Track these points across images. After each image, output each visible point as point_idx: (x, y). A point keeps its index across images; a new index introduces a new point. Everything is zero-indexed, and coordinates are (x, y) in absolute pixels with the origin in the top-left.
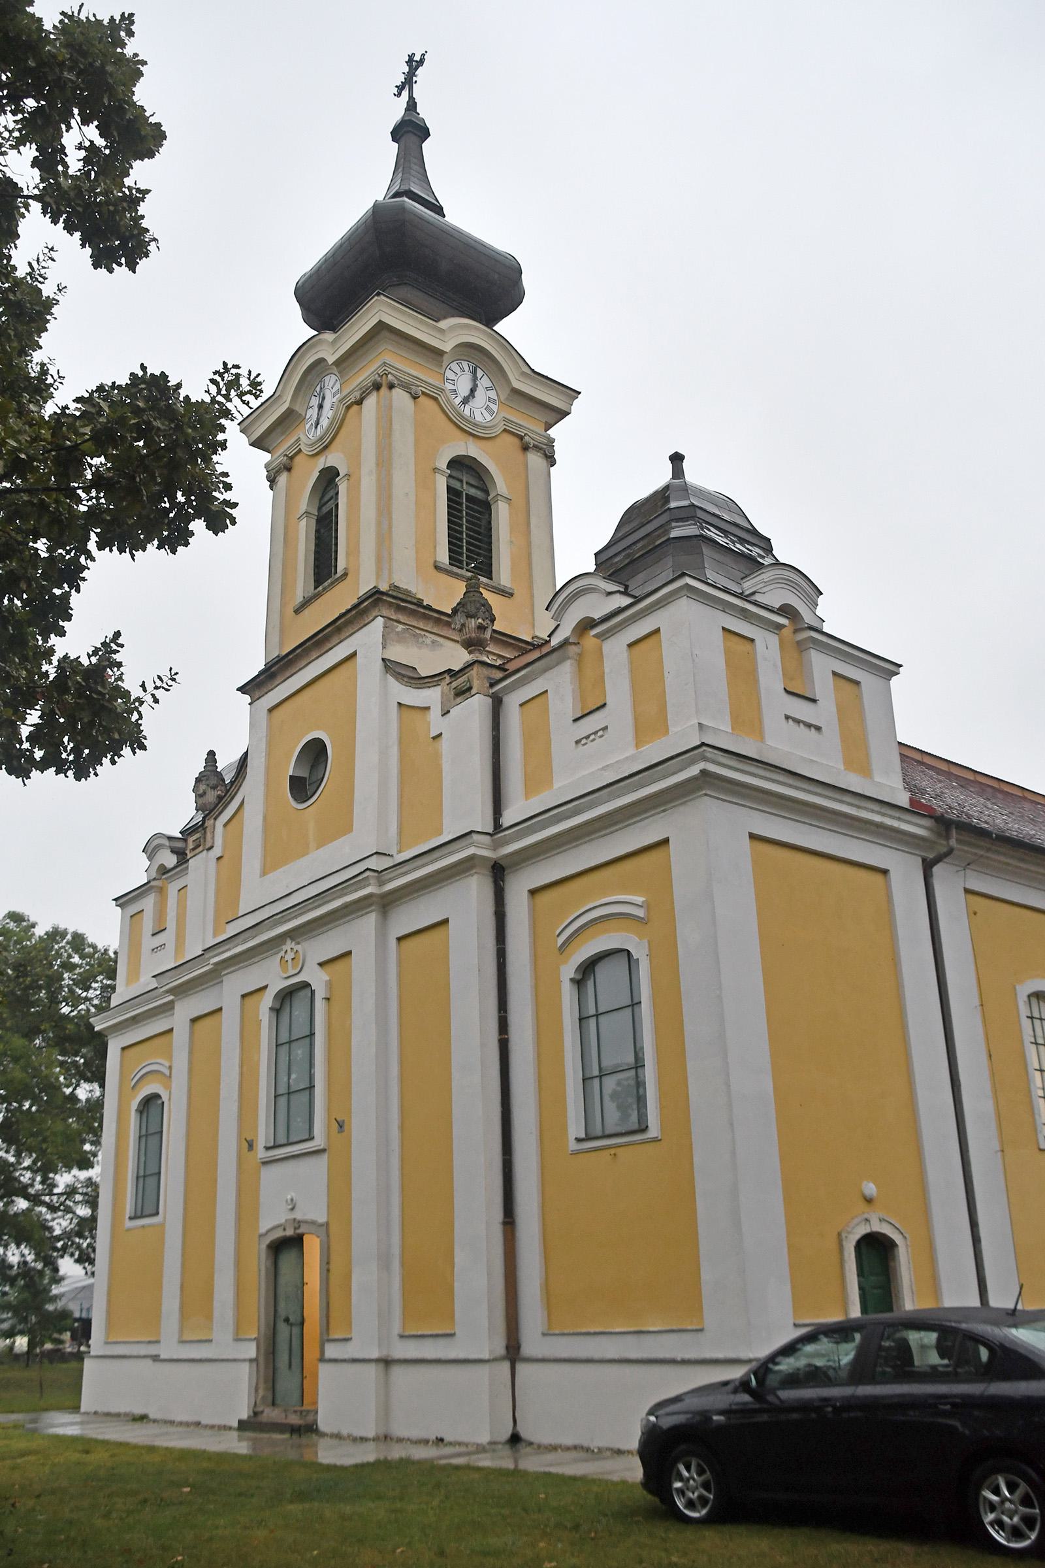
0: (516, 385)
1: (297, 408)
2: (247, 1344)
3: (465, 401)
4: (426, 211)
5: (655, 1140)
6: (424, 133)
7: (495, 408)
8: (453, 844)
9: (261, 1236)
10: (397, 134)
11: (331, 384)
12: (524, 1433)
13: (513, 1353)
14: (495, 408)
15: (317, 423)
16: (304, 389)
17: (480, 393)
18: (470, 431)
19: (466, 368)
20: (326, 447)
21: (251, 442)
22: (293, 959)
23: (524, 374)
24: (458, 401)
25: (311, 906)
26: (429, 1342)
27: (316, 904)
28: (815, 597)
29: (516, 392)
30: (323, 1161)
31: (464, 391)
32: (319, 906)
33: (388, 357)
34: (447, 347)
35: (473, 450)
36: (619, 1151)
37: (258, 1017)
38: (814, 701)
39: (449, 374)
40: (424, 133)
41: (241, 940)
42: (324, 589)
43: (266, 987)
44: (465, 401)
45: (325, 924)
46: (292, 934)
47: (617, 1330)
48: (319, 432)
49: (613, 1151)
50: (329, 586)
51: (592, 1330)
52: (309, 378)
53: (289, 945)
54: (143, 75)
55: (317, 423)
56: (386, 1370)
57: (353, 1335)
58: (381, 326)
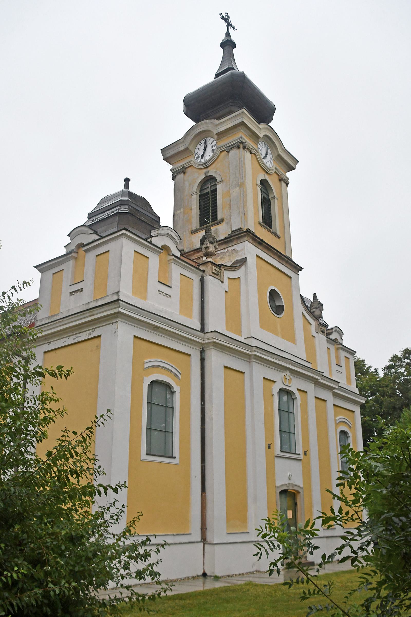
0: (280, 153)
1: (190, 148)
3: (264, 158)
4: (224, 75)
6: (234, 45)
10: (223, 45)
11: (210, 142)
12: (201, 573)
13: (204, 540)
15: (202, 156)
17: (268, 155)
18: (266, 171)
19: (264, 145)
21: (164, 158)
23: (283, 149)
24: (262, 157)
25: (304, 368)
27: (305, 369)
29: (279, 156)
31: (264, 154)
32: (305, 370)
33: (242, 135)
34: (261, 135)
35: (267, 177)
39: (259, 146)
40: (234, 45)
44: (264, 158)
45: (301, 376)
48: (203, 160)
55: (202, 156)
58: (243, 124)
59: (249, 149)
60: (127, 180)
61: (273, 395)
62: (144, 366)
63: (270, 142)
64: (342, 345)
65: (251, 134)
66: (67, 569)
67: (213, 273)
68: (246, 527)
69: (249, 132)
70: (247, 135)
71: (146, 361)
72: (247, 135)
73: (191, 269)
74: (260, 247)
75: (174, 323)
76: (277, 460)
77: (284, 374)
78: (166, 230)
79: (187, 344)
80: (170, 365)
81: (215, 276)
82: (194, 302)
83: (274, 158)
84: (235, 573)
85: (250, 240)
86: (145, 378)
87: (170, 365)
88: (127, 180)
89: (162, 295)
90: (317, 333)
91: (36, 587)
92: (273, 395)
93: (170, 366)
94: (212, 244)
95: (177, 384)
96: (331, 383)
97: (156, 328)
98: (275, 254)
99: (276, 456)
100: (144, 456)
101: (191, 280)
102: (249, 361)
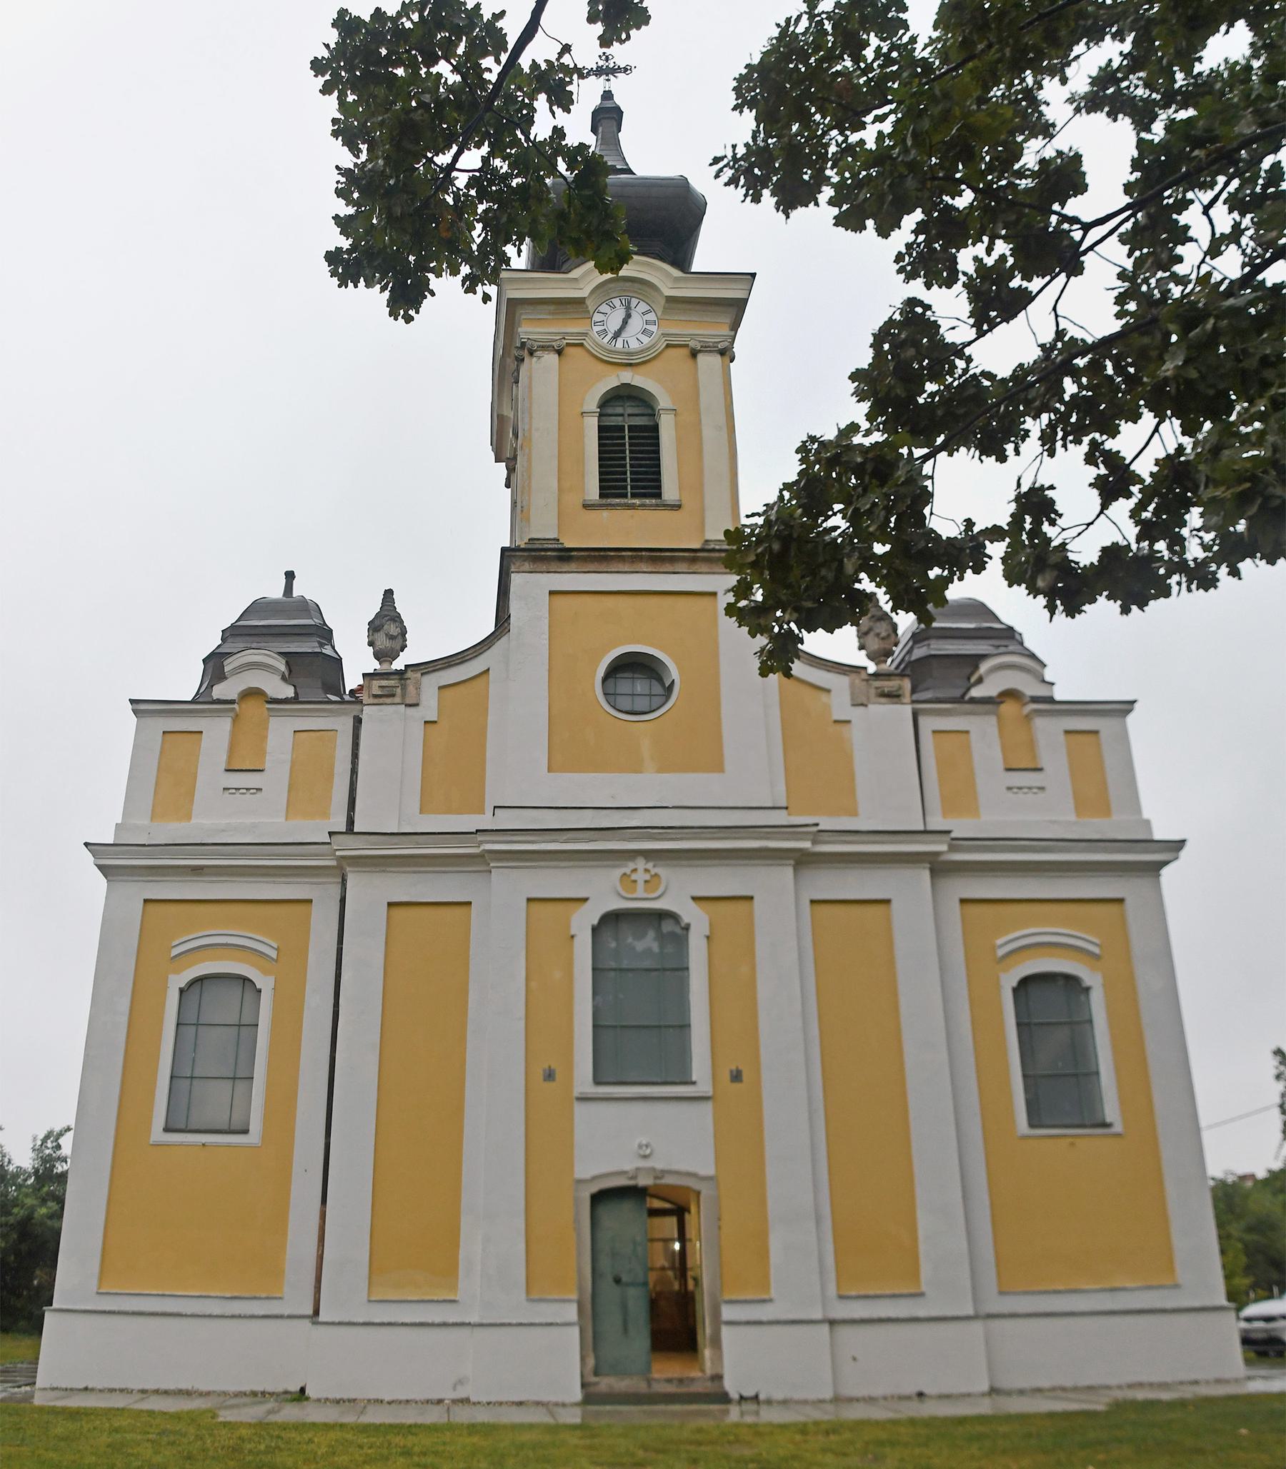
2: (567, 1305)
5: (1118, 1135)
7: (653, 328)
8: (882, 835)
9: (580, 1182)
14: (653, 328)
16: (602, 290)
20: (631, 365)
22: (646, 882)
26: (903, 1302)
28: (658, 501)
29: (670, 299)
30: (707, 1107)
32: (681, 839)
36: (1078, 1141)
37: (568, 926)
38: (1040, 770)
41: (565, 838)
42: (643, 505)
43: (586, 900)
46: (648, 854)
47: (179, 1294)
49: (1070, 1140)
50: (651, 506)
51: (871, 1292)
52: (612, 285)
53: (641, 864)
54: (1135, 422)
56: (831, 1329)
57: (773, 1293)
59: (549, 347)
60: (290, 576)
61: (573, 937)
62: (170, 953)
63: (636, 285)
64: (1050, 700)
65: (552, 308)
66: (227, 1442)
67: (375, 696)
68: (454, 1287)
69: (545, 307)
70: (545, 317)
71: (999, 942)
72: (545, 317)
73: (318, 710)
74: (573, 566)
75: (231, 847)
76: (580, 1110)
77: (618, 872)
78: (241, 659)
79: (752, 862)
80: (250, 938)
81: (381, 700)
82: (336, 780)
83: (659, 314)
84: (368, 1398)
85: (527, 566)
86: (171, 977)
87: (250, 938)
88: (290, 576)
89: (238, 795)
90: (862, 708)
91: (142, 1466)
92: (573, 937)
93: (245, 939)
94: (379, 630)
95: (266, 972)
96: (901, 842)
97: (197, 870)
98: (633, 560)
99: (579, 1099)
100: (157, 1134)
101: (332, 732)
102: (486, 868)
